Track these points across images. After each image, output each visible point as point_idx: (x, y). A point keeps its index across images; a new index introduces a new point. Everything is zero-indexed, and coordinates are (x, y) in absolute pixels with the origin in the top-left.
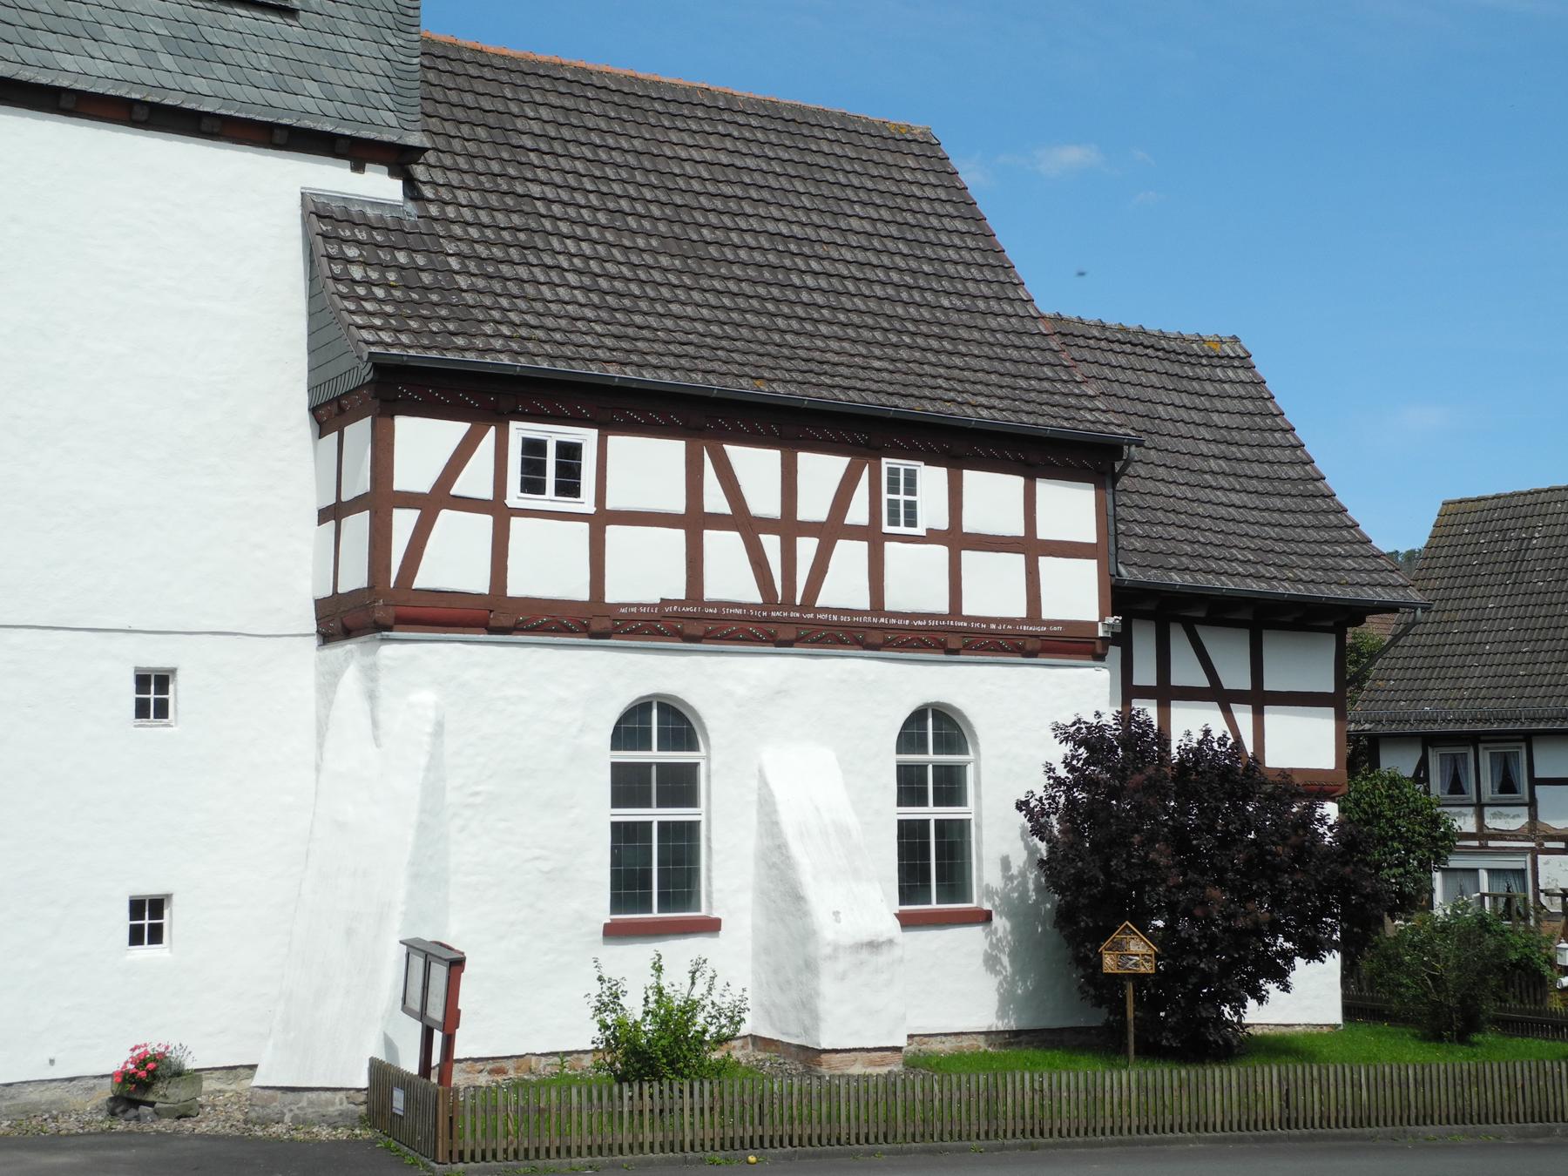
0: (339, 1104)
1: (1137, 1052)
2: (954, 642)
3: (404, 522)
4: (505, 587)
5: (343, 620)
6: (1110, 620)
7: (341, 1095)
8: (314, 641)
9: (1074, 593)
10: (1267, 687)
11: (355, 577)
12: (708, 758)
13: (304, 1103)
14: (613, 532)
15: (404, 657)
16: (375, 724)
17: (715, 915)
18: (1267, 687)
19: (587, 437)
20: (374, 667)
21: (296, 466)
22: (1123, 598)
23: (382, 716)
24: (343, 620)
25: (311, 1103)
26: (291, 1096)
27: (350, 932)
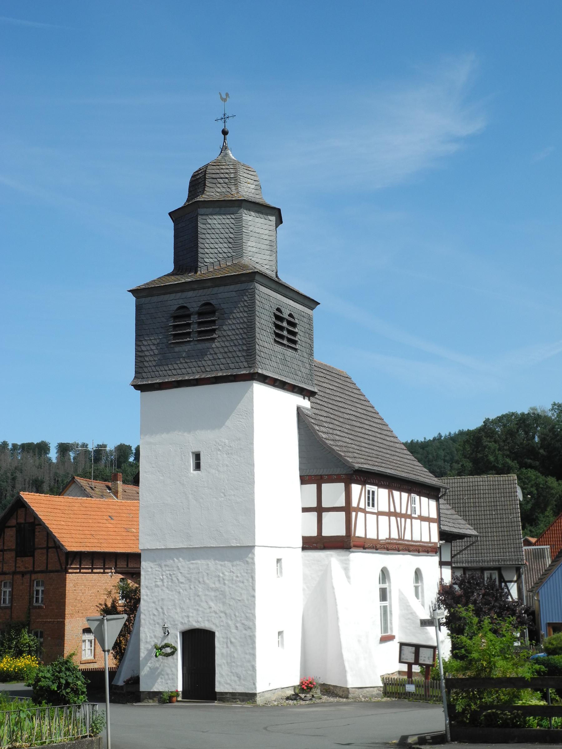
0: (375, 691)
1: (110, 702)
2: (411, 548)
3: (354, 514)
4: (343, 536)
5: (311, 544)
6: (441, 542)
7: (376, 689)
8: (301, 549)
9: (429, 534)
10: (344, 505)
11: (314, 533)
12: (390, 586)
13: (365, 692)
14: (324, 505)
15: (357, 558)
16: (348, 577)
17: (394, 634)
18: (344, 505)
19: (374, 488)
20: (348, 560)
21: (300, 495)
22: (443, 535)
23: (351, 574)
24: (311, 544)
25: (368, 692)
26: (360, 690)
27: (359, 641)
